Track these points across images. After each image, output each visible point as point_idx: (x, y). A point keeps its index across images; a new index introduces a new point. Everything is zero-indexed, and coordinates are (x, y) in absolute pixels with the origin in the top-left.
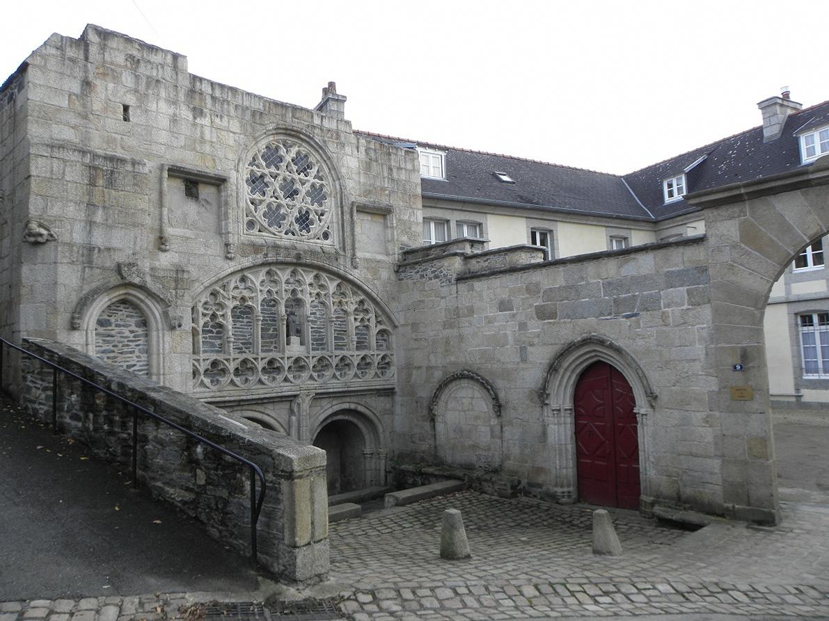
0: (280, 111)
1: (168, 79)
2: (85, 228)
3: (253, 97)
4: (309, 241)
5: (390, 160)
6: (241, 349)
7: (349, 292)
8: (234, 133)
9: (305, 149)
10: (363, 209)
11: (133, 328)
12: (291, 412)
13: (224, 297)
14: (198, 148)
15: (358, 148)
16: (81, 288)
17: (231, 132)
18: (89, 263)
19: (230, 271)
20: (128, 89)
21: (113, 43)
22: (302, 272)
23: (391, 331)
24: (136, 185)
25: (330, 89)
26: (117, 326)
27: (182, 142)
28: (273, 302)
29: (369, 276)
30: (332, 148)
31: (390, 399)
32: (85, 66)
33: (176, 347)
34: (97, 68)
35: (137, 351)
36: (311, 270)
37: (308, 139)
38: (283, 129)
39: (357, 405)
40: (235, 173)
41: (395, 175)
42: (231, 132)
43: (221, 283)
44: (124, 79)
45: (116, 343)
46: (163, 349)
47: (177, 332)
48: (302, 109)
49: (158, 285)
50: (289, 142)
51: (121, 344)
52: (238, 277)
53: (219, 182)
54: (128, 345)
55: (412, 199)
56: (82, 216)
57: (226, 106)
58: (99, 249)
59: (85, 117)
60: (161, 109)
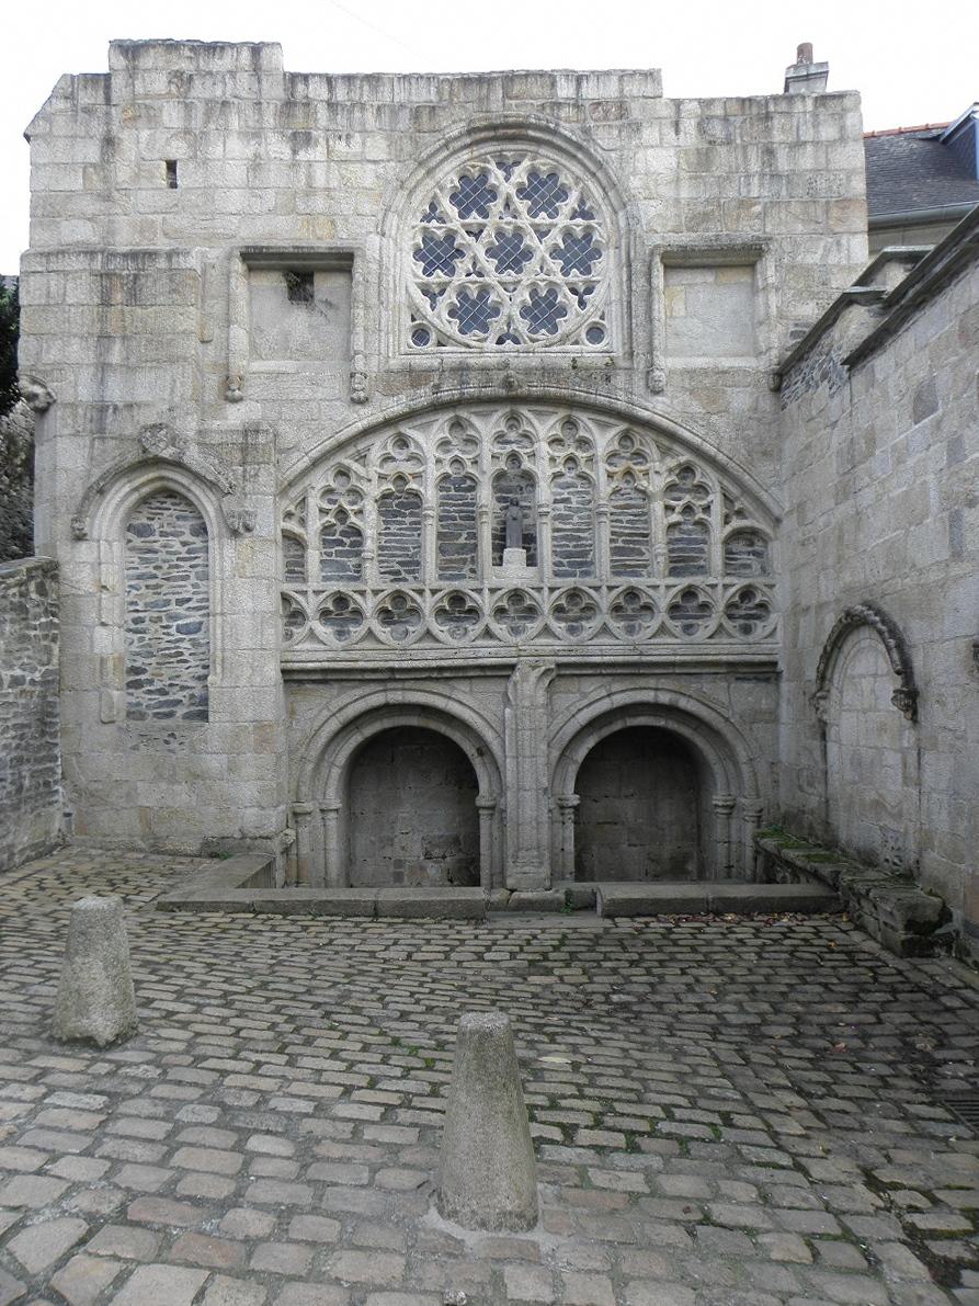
0: (474, 92)
1: (244, 94)
2: (95, 375)
3: (413, 81)
4: (565, 348)
5: (768, 130)
6: (398, 573)
7: (652, 451)
8: (375, 162)
9: (545, 160)
10: (678, 261)
11: (187, 537)
12: (507, 702)
13: (360, 478)
14: (301, 207)
15: (677, 126)
16: (89, 476)
17: (369, 161)
18: (100, 432)
19: (360, 426)
20: (172, 132)
21: (147, 61)
22: (530, 415)
23: (768, 530)
24: (174, 290)
25: (804, 51)
26: (163, 534)
27: (270, 199)
28: (469, 482)
29: (696, 408)
30: (606, 140)
31: (770, 687)
32: (108, 114)
33: (244, 567)
34: (124, 111)
35: (192, 575)
36: (551, 409)
37: (547, 137)
38: (486, 128)
39: (677, 696)
40: (377, 238)
41: (783, 163)
42: (369, 161)
43: (351, 450)
44: (165, 118)
45: (159, 563)
46: (222, 571)
47: (246, 541)
48: (527, 75)
49: (211, 459)
50: (508, 154)
51: (167, 565)
52: (387, 436)
53: (342, 261)
54: (177, 566)
55: (835, 212)
56: (91, 357)
57: (357, 114)
58: (116, 408)
59: (107, 198)
60: (229, 152)
